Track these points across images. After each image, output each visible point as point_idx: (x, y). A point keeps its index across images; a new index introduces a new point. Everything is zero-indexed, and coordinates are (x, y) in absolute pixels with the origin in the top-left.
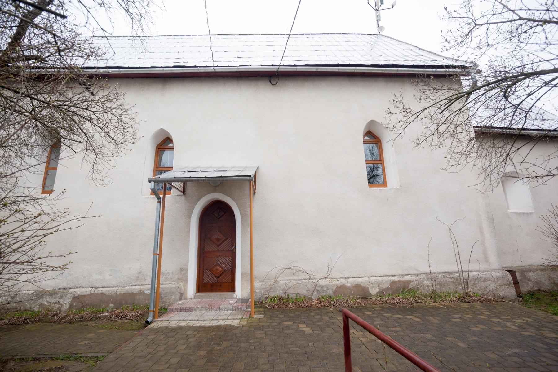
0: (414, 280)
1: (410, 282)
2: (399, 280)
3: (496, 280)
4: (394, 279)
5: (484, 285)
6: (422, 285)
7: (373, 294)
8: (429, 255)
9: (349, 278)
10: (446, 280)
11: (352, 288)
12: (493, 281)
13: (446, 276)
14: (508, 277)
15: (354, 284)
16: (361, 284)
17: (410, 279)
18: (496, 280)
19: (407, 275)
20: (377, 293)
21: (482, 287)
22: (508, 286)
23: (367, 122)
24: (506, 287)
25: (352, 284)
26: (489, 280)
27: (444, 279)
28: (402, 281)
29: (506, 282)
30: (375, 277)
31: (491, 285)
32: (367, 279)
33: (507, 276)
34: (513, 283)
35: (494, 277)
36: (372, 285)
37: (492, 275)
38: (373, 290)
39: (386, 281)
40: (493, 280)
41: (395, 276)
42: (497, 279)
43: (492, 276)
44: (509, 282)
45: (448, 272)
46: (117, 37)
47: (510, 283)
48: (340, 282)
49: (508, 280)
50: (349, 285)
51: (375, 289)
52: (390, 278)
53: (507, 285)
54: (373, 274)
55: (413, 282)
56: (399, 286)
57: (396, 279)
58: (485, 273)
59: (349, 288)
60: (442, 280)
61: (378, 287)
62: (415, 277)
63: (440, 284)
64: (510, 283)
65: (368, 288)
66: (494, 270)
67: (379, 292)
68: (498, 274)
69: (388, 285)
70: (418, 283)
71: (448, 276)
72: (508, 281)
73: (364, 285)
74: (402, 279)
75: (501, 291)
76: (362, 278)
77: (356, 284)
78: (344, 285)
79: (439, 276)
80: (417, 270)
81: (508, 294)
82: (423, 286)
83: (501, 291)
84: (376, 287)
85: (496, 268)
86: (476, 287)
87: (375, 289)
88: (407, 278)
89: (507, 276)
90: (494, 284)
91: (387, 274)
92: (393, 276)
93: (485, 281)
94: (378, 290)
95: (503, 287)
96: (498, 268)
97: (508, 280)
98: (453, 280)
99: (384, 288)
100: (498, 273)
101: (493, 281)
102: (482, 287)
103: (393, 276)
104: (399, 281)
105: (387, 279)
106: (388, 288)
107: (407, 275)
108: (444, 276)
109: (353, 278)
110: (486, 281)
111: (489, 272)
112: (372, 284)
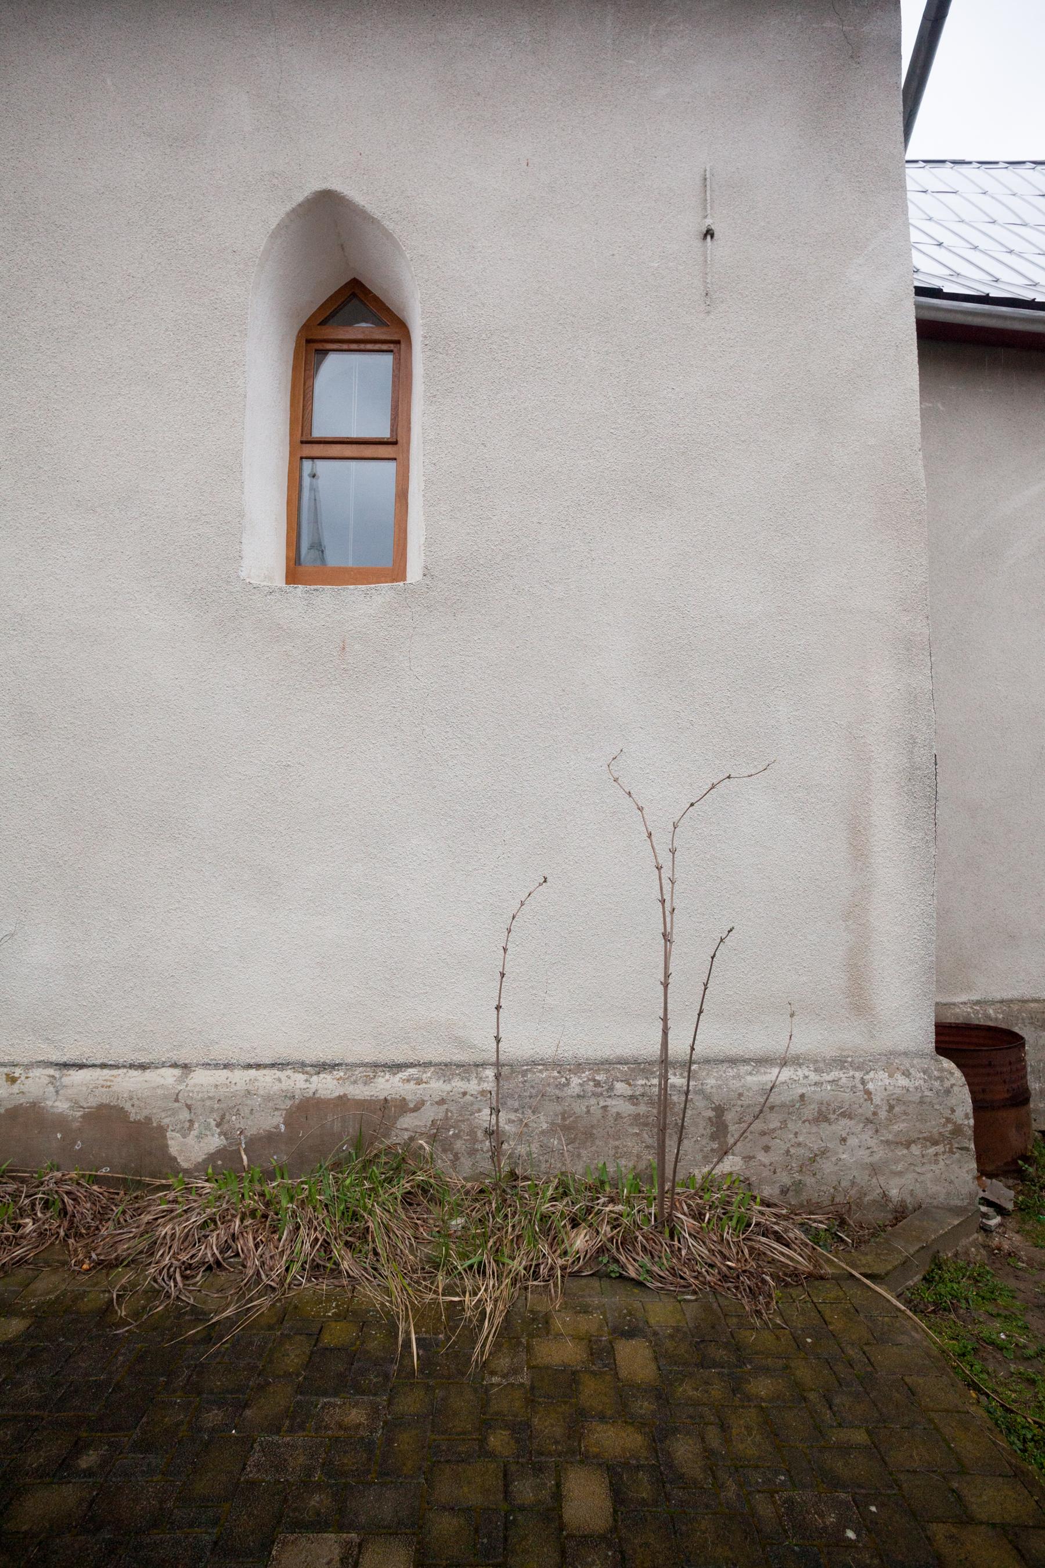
0: (423, 1103)
1: (402, 1106)
2: (340, 1097)
3: (883, 1114)
4: (313, 1087)
5: (811, 1138)
6: (464, 1126)
7: (185, 1165)
8: (503, 975)
9: (81, 1066)
10: (605, 1107)
11: (76, 1125)
12: (868, 1121)
13: (611, 1088)
14: (952, 1101)
15: (93, 1102)
16: (128, 1107)
17: (403, 1093)
18: (883, 1114)
19: (396, 1067)
20: (212, 1158)
21: (801, 1151)
22: (940, 1148)
23: (289, 207)
24: (932, 1150)
25: (76, 1105)
26: (843, 1115)
27: (593, 1101)
28: (362, 1104)
29: (934, 1126)
30: (226, 1066)
31: (853, 1141)
32: (168, 1077)
33: (948, 1092)
34: (970, 1132)
35: (877, 1100)
36: (185, 1115)
37: (870, 1086)
38: (191, 1140)
39: (268, 1098)
40: (869, 1115)
41: (334, 1066)
42: (891, 1108)
43: (868, 1093)
44: (950, 1127)
45: (636, 1062)
46: (954, 162)
47: (957, 1131)
48: (15, 1088)
49: (947, 1113)
50: (62, 1106)
51: (199, 1137)
52: (297, 1082)
53: (935, 1143)
54: (218, 1054)
55: (416, 1109)
56: (337, 1127)
57: (327, 1086)
58: (835, 1074)
59: (60, 1122)
60: (580, 1108)
61: (218, 1125)
62: (437, 1087)
63: (566, 1129)
64: (957, 1131)
65: (162, 1130)
66: (890, 1061)
67: (220, 1153)
68: (903, 1081)
69: (274, 1121)
70: (447, 1118)
71: (620, 1087)
72: (948, 1120)
73: (146, 1112)
74: (359, 1091)
75: (900, 1174)
76: (149, 1074)
77: (101, 1107)
78: (34, 1105)
79: (575, 1081)
80: (461, 1043)
81: (933, 1189)
82: (472, 1133)
83: (900, 1174)
84: (208, 1127)
85: (901, 1048)
86: (767, 1149)
87: (199, 1137)
88: (387, 1086)
89: (948, 1092)
90: (867, 1137)
91: (296, 1056)
92: (323, 1067)
93: (822, 1117)
94: (215, 1142)
95: (915, 1150)
96: (912, 1047)
97: (947, 1113)
98: (642, 1109)
99: (251, 1132)
100: (907, 1074)
101: (868, 1121)
102: (801, 1151)
103: (323, 1067)
104: (342, 1099)
105: (277, 1087)
106: (270, 1138)
107: (396, 1067)
108: (598, 1084)
109: (103, 1066)
110: (826, 1120)
111: (858, 1068)
112: (189, 1107)
